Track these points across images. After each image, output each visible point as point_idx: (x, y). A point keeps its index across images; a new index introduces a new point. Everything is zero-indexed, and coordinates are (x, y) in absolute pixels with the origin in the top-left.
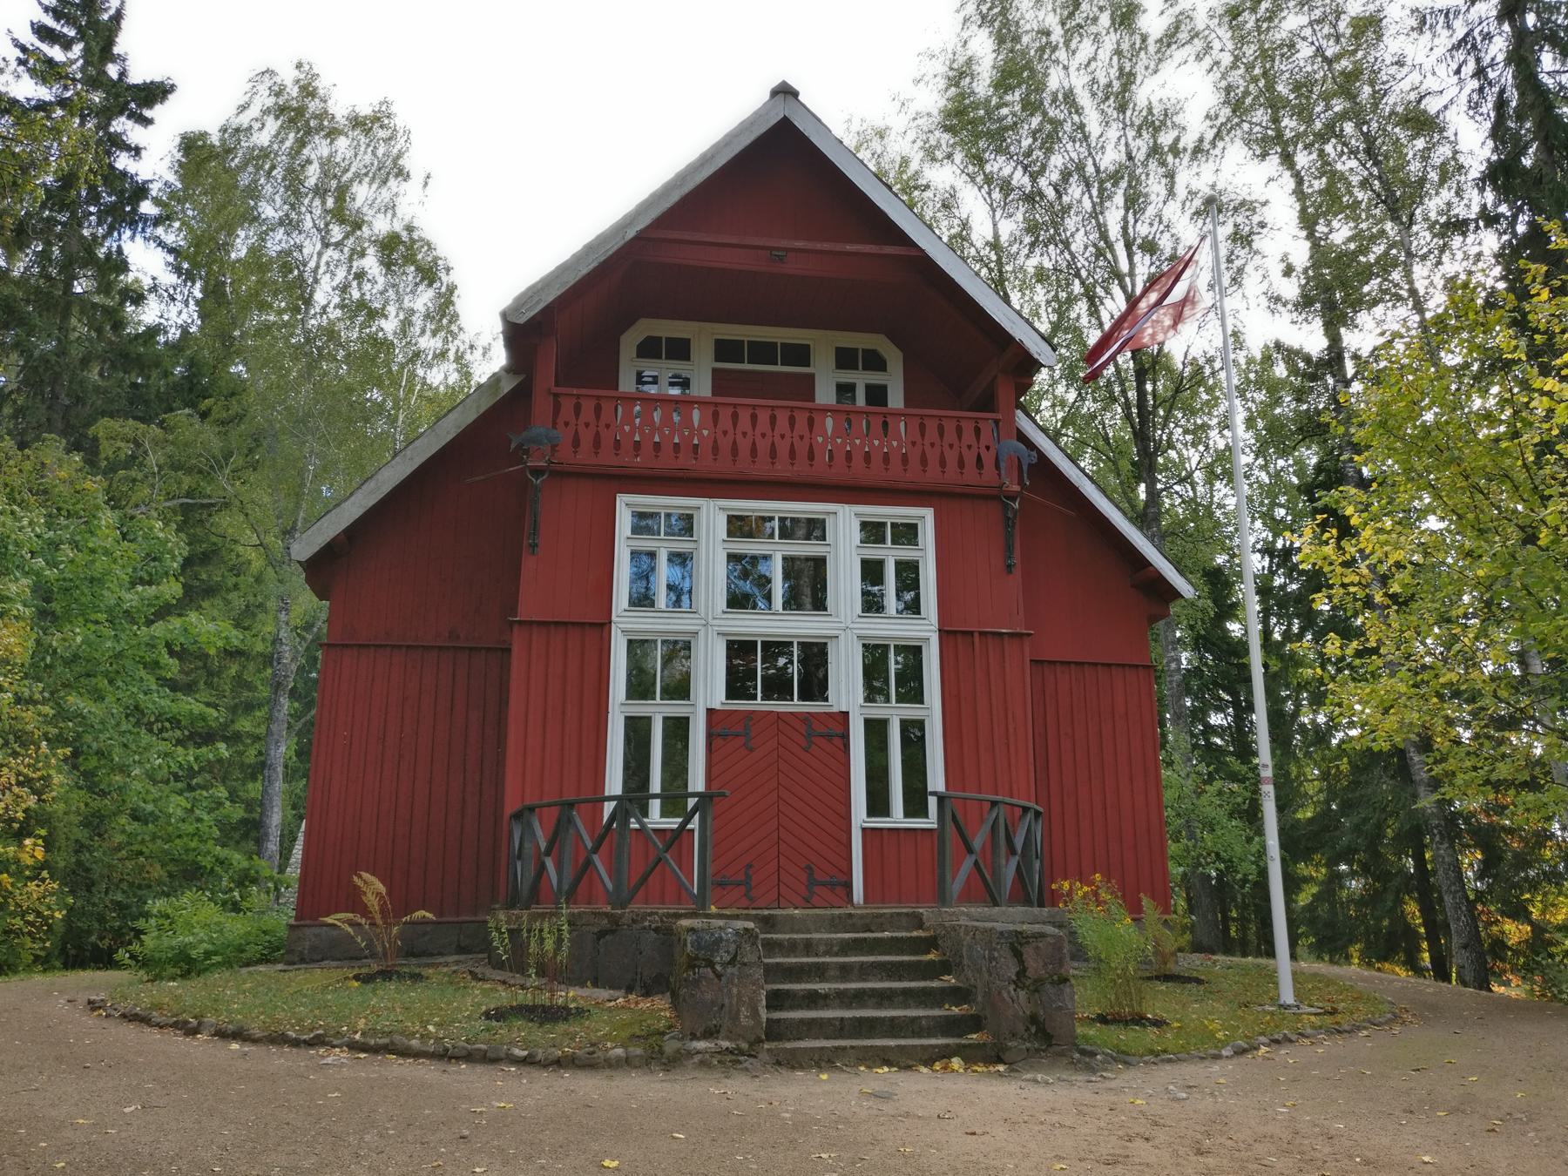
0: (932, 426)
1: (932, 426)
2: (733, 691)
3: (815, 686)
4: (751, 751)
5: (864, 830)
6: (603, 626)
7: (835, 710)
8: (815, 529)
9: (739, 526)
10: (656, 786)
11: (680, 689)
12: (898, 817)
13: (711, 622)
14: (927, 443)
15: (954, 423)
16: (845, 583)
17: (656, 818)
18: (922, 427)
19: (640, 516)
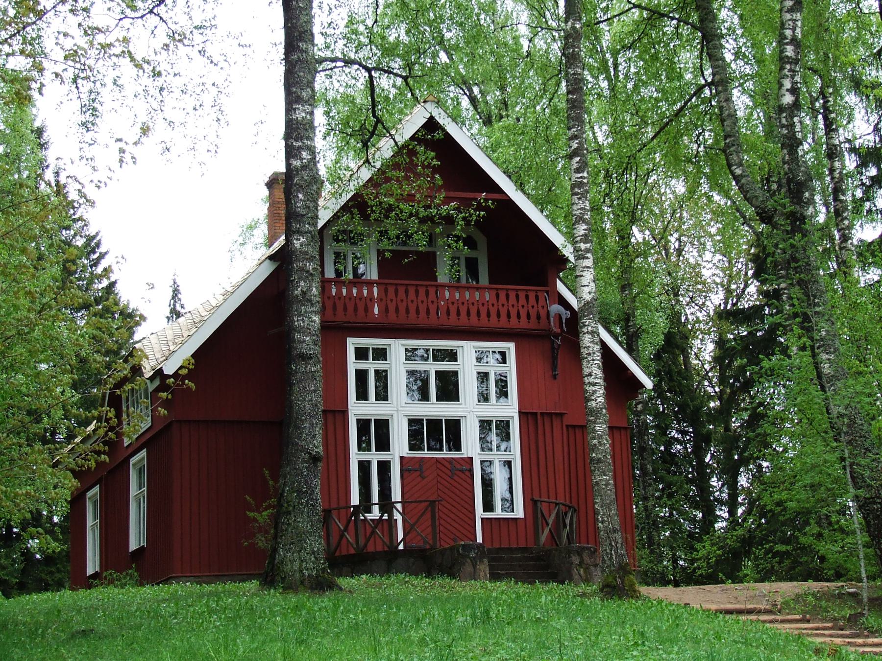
0: (502, 295)
1: (502, 295)
2: (412, 448)
3: (455, 443)
4: (423, 478)
5: (482, 519)
6: (344, 413)
7: (465, 456)
8: (452, 356)
9: (411, 353)
10: (375, 498)
11: (384, 444)
12: (498, 513)
13: (400, 409)
14: (419, 301)
15: (424, 289)
16: (468, 386)
17: (375, 513)
18: (497, 296)
19: (357, 350)
